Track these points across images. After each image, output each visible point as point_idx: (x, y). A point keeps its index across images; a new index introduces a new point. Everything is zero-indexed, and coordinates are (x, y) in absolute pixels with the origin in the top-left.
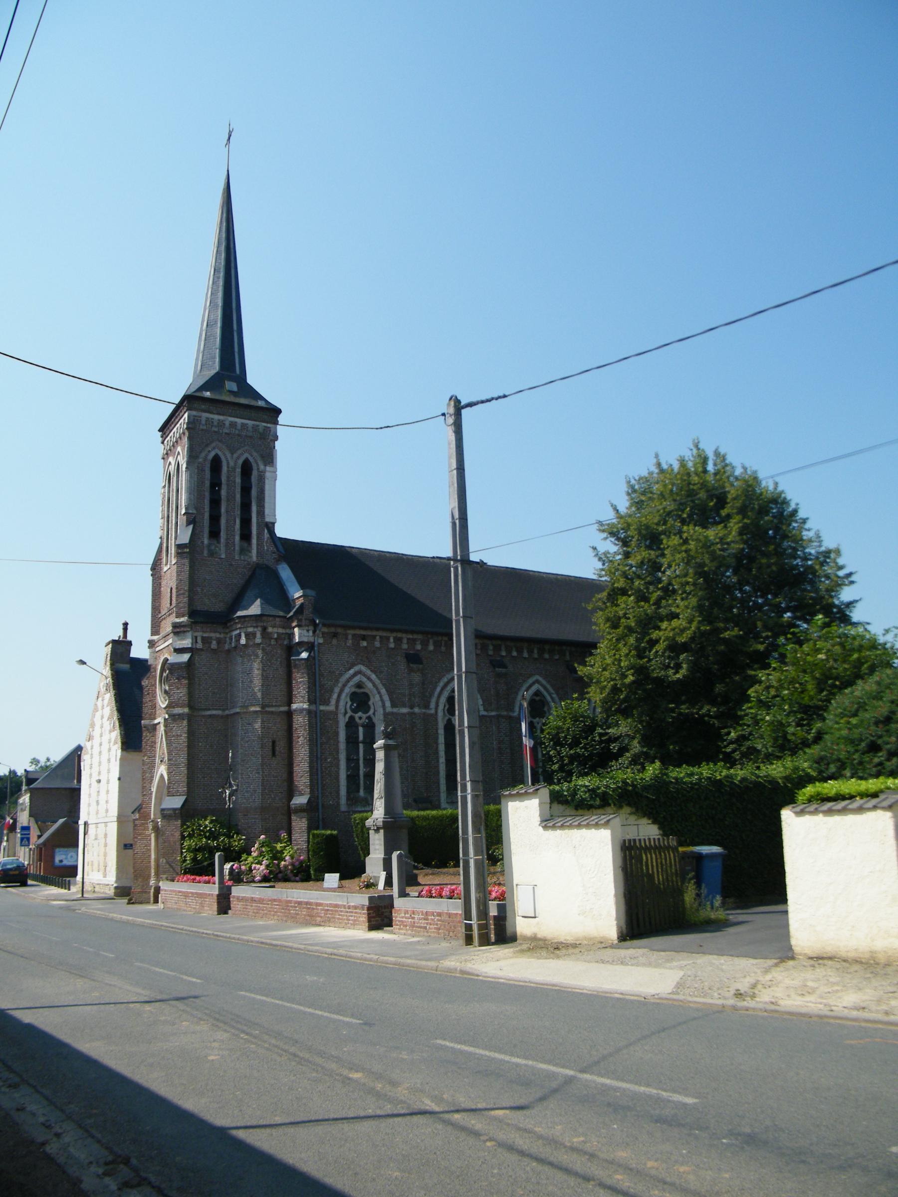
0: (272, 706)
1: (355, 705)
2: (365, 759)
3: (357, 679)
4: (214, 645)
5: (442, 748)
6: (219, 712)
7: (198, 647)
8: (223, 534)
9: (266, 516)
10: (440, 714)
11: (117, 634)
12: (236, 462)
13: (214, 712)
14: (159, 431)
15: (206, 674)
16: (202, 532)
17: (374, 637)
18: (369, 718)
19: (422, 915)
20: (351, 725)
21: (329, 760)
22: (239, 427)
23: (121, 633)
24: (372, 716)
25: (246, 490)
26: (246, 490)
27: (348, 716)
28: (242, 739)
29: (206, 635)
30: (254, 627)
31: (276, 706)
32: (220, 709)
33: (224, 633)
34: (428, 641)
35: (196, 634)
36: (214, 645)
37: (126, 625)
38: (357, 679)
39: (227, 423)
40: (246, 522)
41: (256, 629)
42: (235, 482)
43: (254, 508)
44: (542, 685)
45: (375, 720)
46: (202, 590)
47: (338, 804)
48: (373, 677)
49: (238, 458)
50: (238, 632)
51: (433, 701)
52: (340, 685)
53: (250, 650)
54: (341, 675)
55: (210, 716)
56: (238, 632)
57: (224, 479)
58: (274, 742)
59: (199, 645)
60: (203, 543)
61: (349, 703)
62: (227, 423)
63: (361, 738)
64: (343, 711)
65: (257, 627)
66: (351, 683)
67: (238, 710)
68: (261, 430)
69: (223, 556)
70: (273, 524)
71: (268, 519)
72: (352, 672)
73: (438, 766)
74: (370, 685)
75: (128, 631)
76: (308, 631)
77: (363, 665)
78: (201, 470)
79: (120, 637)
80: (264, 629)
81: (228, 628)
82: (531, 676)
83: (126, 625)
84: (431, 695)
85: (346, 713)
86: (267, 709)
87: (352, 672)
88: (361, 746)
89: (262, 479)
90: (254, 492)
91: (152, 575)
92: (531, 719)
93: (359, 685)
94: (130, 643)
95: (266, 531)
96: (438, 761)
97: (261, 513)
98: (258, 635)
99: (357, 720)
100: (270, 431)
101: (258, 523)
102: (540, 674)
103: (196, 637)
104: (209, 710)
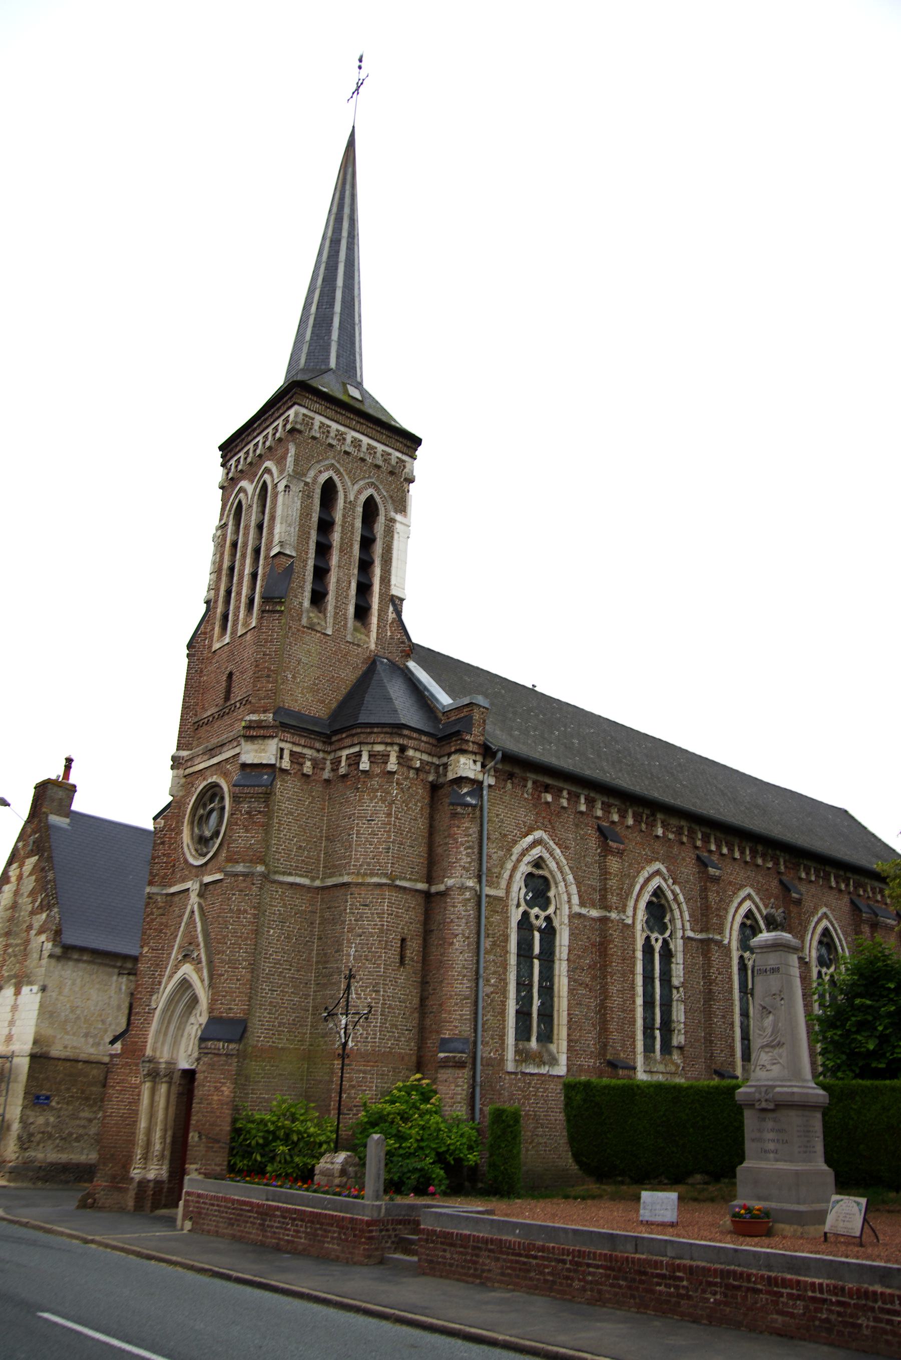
0: (405, 879)
1: (530, 895)
2: (540, 986)
3: (536, 852)
4: (308, 767)
5: (639, 980)
6: (305, 881)
7: (283, 767)
8: (331, 598)
9: (392, 587)
10: (639, 927)
11: (55, 771)
12: (356, 498)
13: (298, 880)
14: (221, 448)
15: (291, 814)
16: (302, 587)
17: (561, 790)
18: (548, 919)
19: (605, 1260)
20: (525, 923)
21: (492, 981)
22: (364, 449)
23: (61, 772)
24: (553, 916)
25: (367, 542)
26: (367, 542)
27: (521, 909)
28: (351, 930)
29: (297, 749)
30: (387, 744)
31: (410, 880)
32: (306, 876)
33: (324, 751)
34: (626, 811)
35: (282, 745)
36: (308, 767)
37: (69, 761)
38: (536, 852)
39: (349, 440)
40: (364, 589)
41: (389, 749)
42: (353, 526)
43: (377, 571)
44: (754, 903)
45: (556, 924)
46: (294, 677)
47: (502, 1060)
48: (558, 851)
49: (360, 492)
50: (356, 749)
51: (631, 903)
52: (514, 858)
53: (375, 782)
54: (515, 842)
55: (292, 885)
56: (356, 749)
57: (338, 516)
58: (403, 940)
59: (286, 764)
60: (301, 604)
61: (524, 891)
62: (349, 440)
63: (537, 950)
64: (515, 902)
65: (392, 744)
66: (527, 859)
67: (346, 879)
68: (393, 462)
69: (329, 632)
70: (402, 600)
71: (394, 591)
72: (530, 839)
73: (633, 1010)
74: (553, 865)
75: (72, 771)
76: (475, 762)
77: (545, 831)
78: (307, 496)
79: (59, 776)
80: (403, 749)
81: (331, 744)
82: (742, 887)
83: (69, 761)
84: (629, 894)
85: (518, 906)
86: (398, 883)
87: (530, 839)
88: (536, 962)
89: (389, 532)
90: (378, 548)
91: (188, 656)
92: (740, 953)
93: (539, 863)
94: (73, 789)
95: (391, 609)
96: (634, 1002)
97: (386, 580)
98: (393, 759)
99: (532, 919)
100: (405, 467)
101: (381, 595)
102: (752, 886)
103: (282, 750)
104: (290, 874)
